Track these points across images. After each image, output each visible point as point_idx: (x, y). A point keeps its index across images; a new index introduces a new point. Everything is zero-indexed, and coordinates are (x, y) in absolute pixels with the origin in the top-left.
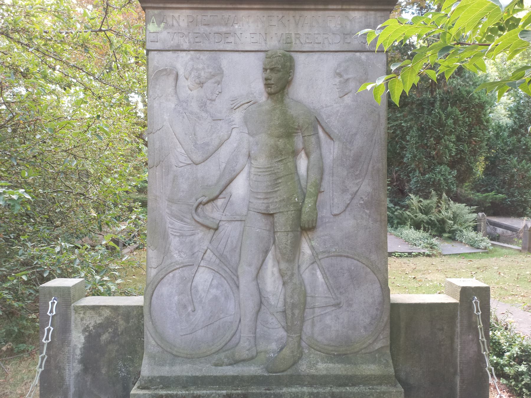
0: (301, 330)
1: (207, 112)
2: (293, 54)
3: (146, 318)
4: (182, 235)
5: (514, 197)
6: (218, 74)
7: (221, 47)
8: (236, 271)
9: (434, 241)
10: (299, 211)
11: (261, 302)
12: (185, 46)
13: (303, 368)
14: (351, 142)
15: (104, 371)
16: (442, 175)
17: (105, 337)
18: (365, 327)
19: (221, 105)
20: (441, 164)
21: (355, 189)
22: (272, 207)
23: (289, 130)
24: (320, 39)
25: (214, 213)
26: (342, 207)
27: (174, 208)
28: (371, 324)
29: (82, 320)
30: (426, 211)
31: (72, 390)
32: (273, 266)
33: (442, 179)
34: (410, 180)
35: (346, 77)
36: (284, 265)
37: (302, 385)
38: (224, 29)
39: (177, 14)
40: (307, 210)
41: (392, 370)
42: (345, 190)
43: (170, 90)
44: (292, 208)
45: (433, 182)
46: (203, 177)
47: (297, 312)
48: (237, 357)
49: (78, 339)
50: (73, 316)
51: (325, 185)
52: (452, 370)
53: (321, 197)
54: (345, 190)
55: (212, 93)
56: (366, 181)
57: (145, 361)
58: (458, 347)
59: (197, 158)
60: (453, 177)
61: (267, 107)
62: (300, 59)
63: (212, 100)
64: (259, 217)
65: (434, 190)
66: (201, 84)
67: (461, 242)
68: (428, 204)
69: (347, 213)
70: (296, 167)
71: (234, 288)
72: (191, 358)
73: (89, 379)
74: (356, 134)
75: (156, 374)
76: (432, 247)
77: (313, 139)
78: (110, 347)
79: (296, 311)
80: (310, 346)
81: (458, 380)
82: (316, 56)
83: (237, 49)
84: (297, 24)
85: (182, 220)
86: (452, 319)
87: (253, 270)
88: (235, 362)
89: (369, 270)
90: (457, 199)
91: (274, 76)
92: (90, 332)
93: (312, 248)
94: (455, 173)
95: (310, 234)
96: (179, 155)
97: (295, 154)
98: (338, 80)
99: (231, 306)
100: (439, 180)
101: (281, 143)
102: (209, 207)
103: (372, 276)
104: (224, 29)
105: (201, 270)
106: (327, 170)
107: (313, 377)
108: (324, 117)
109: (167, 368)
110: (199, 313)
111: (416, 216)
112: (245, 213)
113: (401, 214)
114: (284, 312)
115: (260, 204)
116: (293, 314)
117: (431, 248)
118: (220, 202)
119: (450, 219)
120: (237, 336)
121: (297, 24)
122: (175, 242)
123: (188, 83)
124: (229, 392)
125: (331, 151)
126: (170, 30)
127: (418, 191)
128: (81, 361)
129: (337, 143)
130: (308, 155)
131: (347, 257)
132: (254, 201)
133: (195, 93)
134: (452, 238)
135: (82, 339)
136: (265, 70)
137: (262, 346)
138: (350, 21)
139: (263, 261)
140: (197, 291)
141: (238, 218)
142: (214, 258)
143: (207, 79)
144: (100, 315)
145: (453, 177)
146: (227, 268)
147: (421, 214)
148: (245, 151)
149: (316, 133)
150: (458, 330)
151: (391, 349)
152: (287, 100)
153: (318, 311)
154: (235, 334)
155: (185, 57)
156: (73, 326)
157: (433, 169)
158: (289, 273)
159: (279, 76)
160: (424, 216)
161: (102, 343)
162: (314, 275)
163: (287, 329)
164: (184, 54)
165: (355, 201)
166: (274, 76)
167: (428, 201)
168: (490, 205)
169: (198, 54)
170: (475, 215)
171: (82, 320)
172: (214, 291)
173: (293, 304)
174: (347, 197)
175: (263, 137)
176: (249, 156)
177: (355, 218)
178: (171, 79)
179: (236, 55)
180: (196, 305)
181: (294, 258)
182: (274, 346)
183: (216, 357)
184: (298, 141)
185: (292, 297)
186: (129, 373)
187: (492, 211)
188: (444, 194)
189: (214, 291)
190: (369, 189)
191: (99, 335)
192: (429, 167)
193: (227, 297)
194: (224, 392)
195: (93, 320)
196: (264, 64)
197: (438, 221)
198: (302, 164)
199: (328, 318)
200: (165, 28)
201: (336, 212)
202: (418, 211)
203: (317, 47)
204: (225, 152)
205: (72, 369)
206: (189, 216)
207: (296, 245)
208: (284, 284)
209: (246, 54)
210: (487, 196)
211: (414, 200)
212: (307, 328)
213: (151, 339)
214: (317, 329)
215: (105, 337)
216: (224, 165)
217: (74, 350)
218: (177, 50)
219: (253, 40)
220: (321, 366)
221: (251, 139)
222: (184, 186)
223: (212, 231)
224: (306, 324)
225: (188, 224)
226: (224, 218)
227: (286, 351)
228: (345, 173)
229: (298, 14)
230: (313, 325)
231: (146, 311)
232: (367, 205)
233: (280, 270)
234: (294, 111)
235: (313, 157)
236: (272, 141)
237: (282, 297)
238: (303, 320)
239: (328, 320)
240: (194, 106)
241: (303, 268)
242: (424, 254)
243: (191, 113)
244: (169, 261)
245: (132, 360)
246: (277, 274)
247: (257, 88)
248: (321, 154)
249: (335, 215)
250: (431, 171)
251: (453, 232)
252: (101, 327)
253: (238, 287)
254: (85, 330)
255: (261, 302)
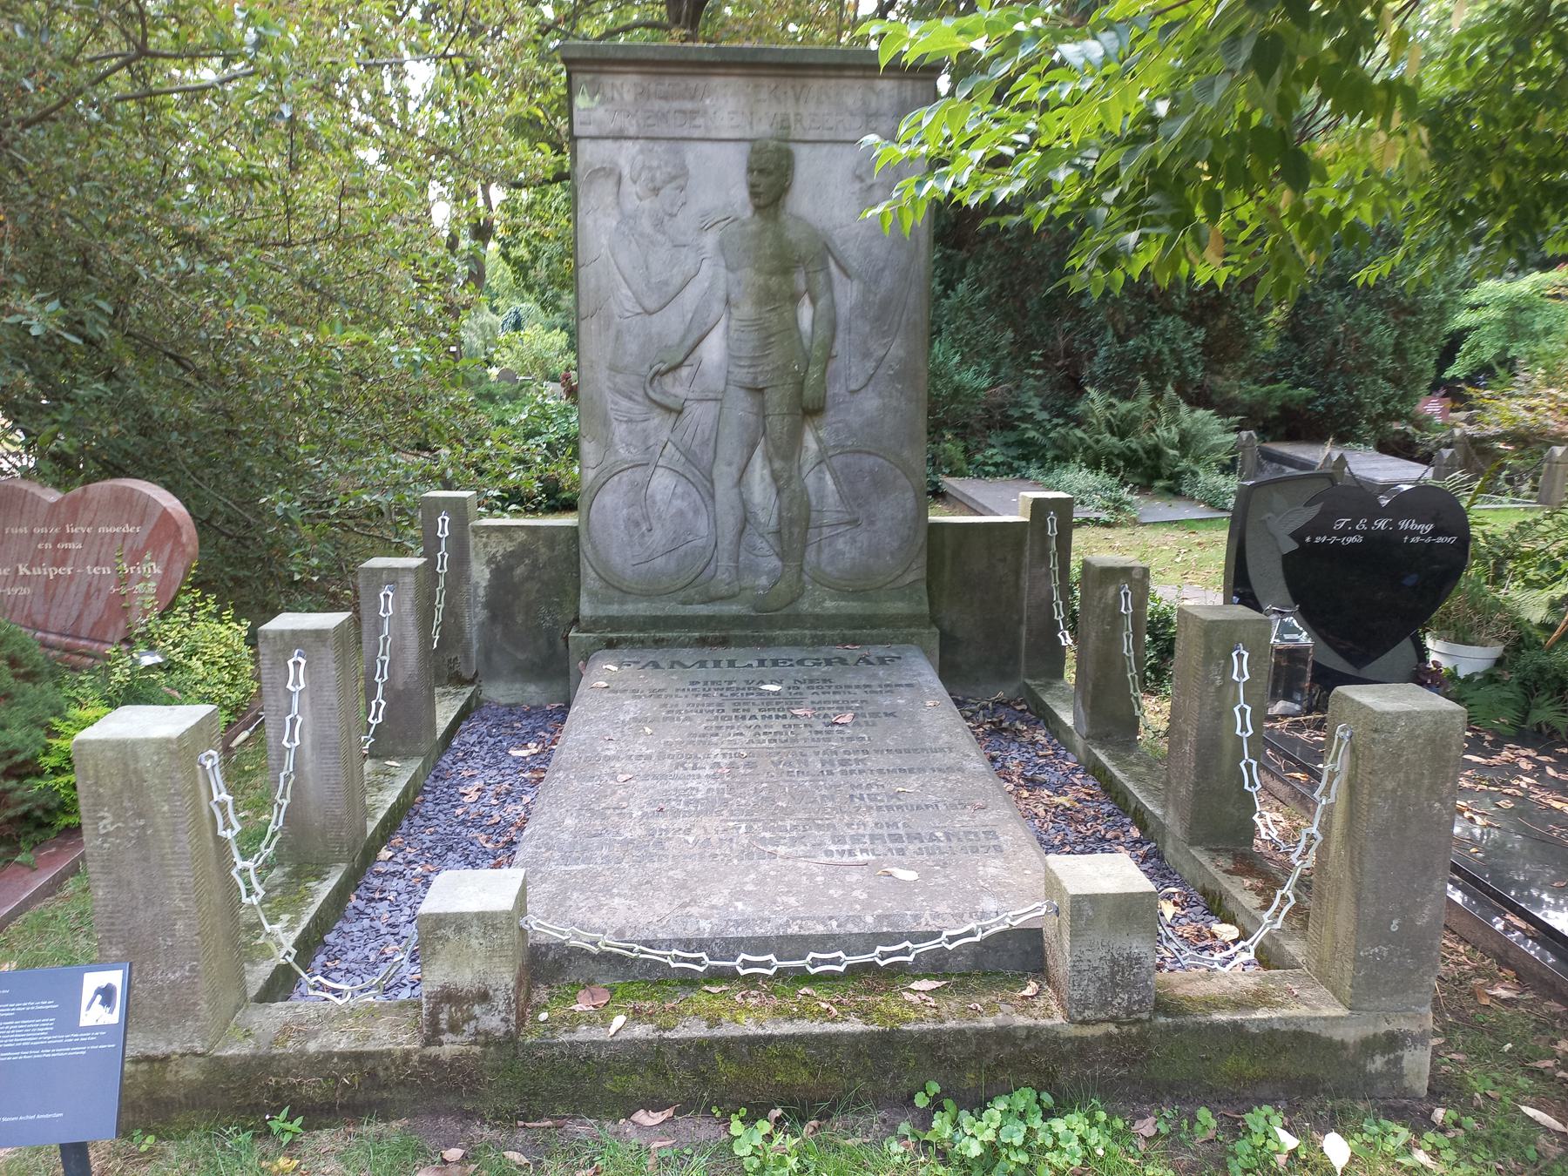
0: (803, 556)
1: (664, 233)
2: (793, 146)
3: (583, 539)
4: (630, 421)
5: (1333, 393)
6: (680, 176)
7: (685, 134)
8: (711, 473)
9: (1124, 493)
10: (800, 384)
11: (746, 519)
12: (632, 131)
13: (805, 606)
14: (876, 282)
15: (519, 619)
16: (1166, 341)
17: (520, 571)
18: (892, 554)
19: (685, 222)
20: (1167, 312)
21: (881, 353)
22: (760, 379)
23: (785, 262)
24: (831, 123)
25: (677, 388)
26: (862, 380)
27: (619, 379)
28: (900, 548)
29: (485, 545)
30: (1122, 428)
31: (475, 646)
32: (763, 467)
33: (1166, 350)
34: (1095, 353)
35: (869, 182)
36: (778, 465)
37: (804, 628)
38: (688, 105)
39: (618, 80)
40: (811, 382)
41: (925, 608)
42: (866, 355)
43: (610, 199)
44: (789, 380)
45: (1145, 357)
46: (659, 334)
47: (796, 530)
48: (713, 592)
49: (480, 574)
50: (472, 540)
51: (838, 347)
52: (1016, 617)
53: (832, 365)
54: (866, 355)
55: (672, 205)
56: (898, 341)
57: (584, 599)
58: (1025, 583)
59: (651, 304)
60: (1196, 345)
61: (753, 227)
62: (802, 153)
63: (672, 216)
64: (742, 393)
65: (1146, 377)
66: (656, 191)
67: (1193, 498)
68: (1129, 412)
69: (870, 388)
70: (796, 320)
71: (709, 502)
72: (648, 595)
73: (498, 630)
74: (883, 270)
75: (601, 613)
76: (1118, 506)
77: (821, 277)
78: (528, 586)
79: (796, 527)
80: (814, 580)
81: (1024, 630)
82: (825, 149)
83: (708, 136)
84: (797, 100)
85: (630, 399)
86: (1019, 546)
87: (734, 471)
88: (711, 600)
89: (899, 472)
90: (1200, 398)
91: (764, 182)
92: (497, 564)
93: (819, 440)
94: (1200, 334)
95: (816, 420)
96: (623, 300)
97: (795, 299)
98: (857, 186)
99: (702, 525)
100: (1159, 352)
101: (774, 282)
102: (668, 379)
103: (903, 481)
104: (688, 105)
105: (659, 471)
106: (841, 327)
107: (817, 617)
108: (838, 242)
109: (616, 607)
110: (658, 533)
111: (1098, 441)
112: (721, 388)
113: (1064, 437)
114: (778, 533)
115: (743, 375)
116: (791, 533)
117: (1117, 509)
118: (685, 372)
119: (1173, 447)
120: (712, 566)
121: (797, 100)
122: (620, 430)
123: (637, 188)
124: (704, 634)
125: (847, 295)
126: (609, 107)
127: (1110, 380)
128: (488, 605)
129: (856, 282)
130: (814, 301)
131: (869, 453)
132: (737, 370)
133: (646, 203)
134: (1174, 492)
135: (487, 575)
136: (750, 170)
137: (747, 581)
138: (878, 95)
139: (749, 458)
140: (654, 502)
141: (711, 395)
142: (678, 455)
143: (666, 182)
144: (511, 539)
145: (1196, 345)
146: (698, 471)
147: (1108, 435)
148: (721, 293)
149: (826, 268)
150: (1027, 560)
151: (929, 588)
152: (784, 217)
153: (826, 532)
154: (708, 564)
155: (631, 148)
156: (472, 554)
157: (1147, 326)
158: (786, 475)
159: (771, 178)
160: (1115, 440)
161: (516, 579)
162: (821, 479)
163: (782, 556)
164: (629, 143)
165: (881, 371)
166: (764, 182)
167: (1129, 405)
168: (1276, 413)
169: (651, 144)
170: (1233, 437)
171: (485, 545)
172: (678, 503)
173: (791, 519)
174: (870, 365)
175: (748, 274)
176: (728, 302)
177: (880, 395)
178: (610, 185)
179: (707, 146)
180: (654, 522)
181: (793, 454)
182: (763, 581)
183: (682, 594)
184: (800, 280)
185: (789, 510)
186: (556, 622)
187: (1282, 430)
188: (1169, 387)
189: (678, 503)
190: (902, 353)
191: (511, 569)
192: (1139, 321)
193: (696, 512)
194: (697, 634)
195: (500, 547)
196: (749, 162)
197: (1147, 452)
198: (806, 314)
199: (841, 540)
200: (602, 103)
201: (853, 387)
202: (1103, 427)
203: (827, 135)
204: (691, 296)
205: (475, 618)
206: (641, 392)
207: (795, 437)
208: (778, 493)
209: (723, 144)
210: (1270, 392)
211: (1095, 401)
212: (811, 555)
213: (590, 570)
214: (825, 556)
215: (520, 571)
216: (690, 316)
217: (476, 589)
218: (619, 137)
219: (733, 123)
220: (828, 604)
221: (731, 276)
222: (633, 347)
223: (674, 416)
224: (809, 549)
225: (638, 403)
226: (691, 396)
227: (782, 585)
228: (868, 329)
229: (798, 82)
230: (819, 550)
231: (582, 530)
232: (897, 377)
233: (773, 472)
234: (793, 234)
235: (821, 303)
236: (761, 280)
237: (775, 512)
238: (805, 545)
239: (840, 544)
240: (646, 225)
241: (806, 469)
242: (1097, 522)
243: (642, 235)
244: (612, 459)
245: (559, 604)
246: (768, 479)
247: (739, 195)
248: (833, 300)
249: (853, 392)
250: (1142, 331)
251: (1176, 477)
252: (513, 557)
253: (713, 497)
254: (489, 562)
255: (746, 519)
